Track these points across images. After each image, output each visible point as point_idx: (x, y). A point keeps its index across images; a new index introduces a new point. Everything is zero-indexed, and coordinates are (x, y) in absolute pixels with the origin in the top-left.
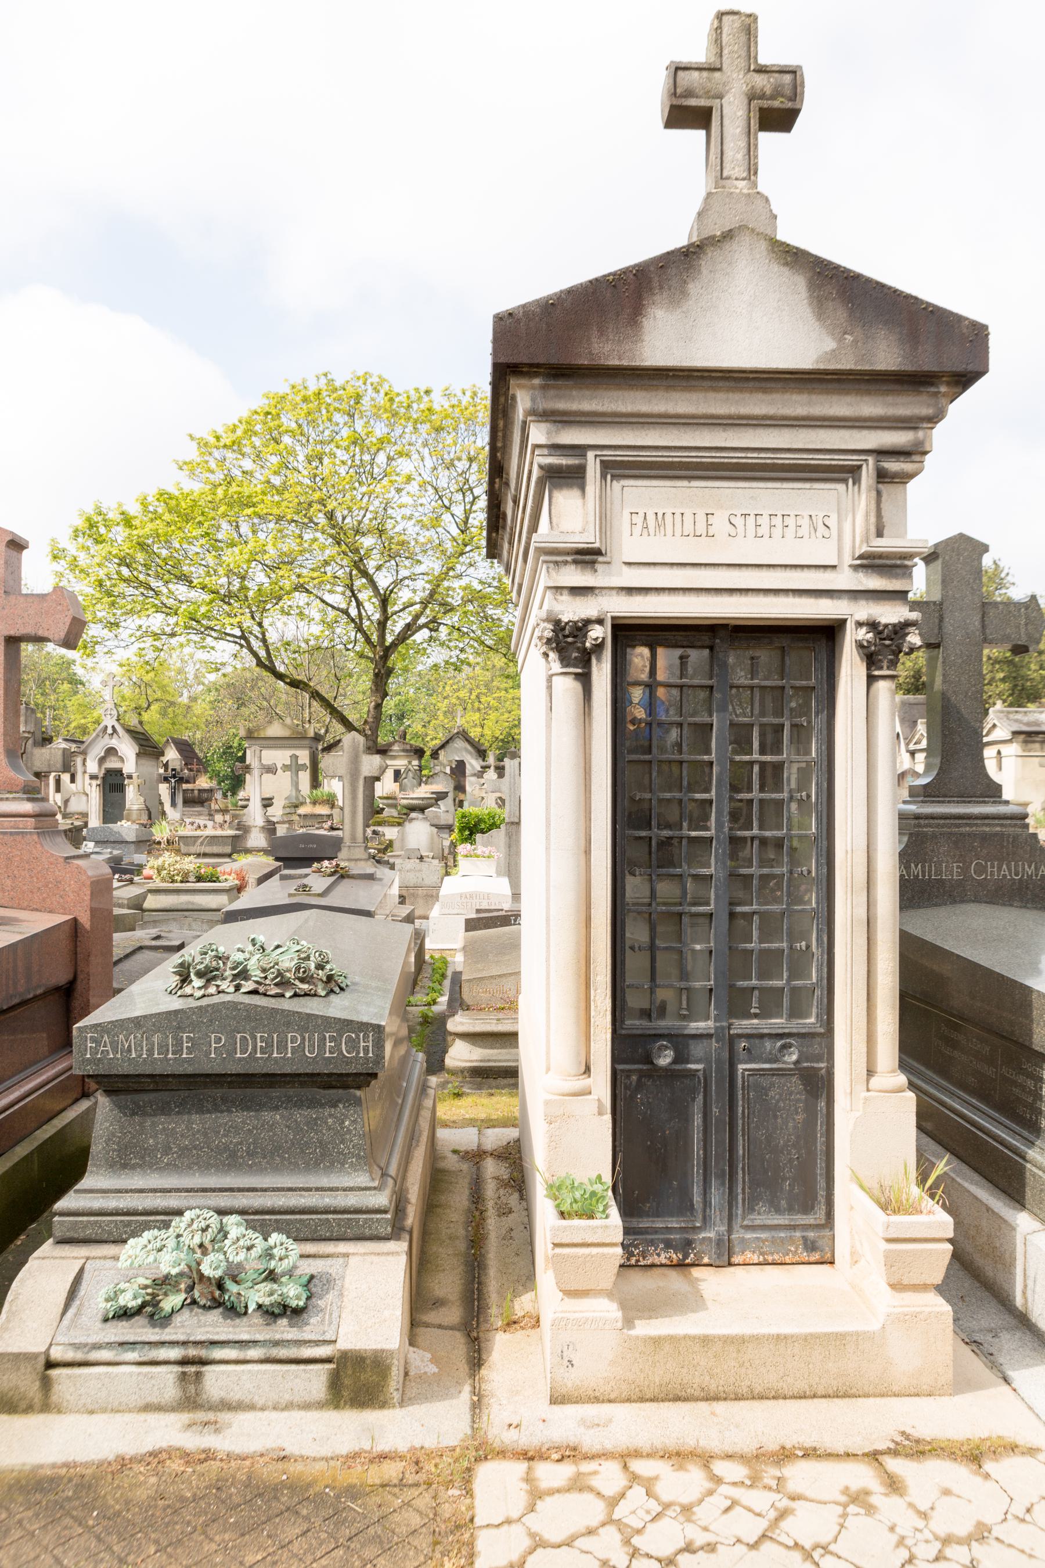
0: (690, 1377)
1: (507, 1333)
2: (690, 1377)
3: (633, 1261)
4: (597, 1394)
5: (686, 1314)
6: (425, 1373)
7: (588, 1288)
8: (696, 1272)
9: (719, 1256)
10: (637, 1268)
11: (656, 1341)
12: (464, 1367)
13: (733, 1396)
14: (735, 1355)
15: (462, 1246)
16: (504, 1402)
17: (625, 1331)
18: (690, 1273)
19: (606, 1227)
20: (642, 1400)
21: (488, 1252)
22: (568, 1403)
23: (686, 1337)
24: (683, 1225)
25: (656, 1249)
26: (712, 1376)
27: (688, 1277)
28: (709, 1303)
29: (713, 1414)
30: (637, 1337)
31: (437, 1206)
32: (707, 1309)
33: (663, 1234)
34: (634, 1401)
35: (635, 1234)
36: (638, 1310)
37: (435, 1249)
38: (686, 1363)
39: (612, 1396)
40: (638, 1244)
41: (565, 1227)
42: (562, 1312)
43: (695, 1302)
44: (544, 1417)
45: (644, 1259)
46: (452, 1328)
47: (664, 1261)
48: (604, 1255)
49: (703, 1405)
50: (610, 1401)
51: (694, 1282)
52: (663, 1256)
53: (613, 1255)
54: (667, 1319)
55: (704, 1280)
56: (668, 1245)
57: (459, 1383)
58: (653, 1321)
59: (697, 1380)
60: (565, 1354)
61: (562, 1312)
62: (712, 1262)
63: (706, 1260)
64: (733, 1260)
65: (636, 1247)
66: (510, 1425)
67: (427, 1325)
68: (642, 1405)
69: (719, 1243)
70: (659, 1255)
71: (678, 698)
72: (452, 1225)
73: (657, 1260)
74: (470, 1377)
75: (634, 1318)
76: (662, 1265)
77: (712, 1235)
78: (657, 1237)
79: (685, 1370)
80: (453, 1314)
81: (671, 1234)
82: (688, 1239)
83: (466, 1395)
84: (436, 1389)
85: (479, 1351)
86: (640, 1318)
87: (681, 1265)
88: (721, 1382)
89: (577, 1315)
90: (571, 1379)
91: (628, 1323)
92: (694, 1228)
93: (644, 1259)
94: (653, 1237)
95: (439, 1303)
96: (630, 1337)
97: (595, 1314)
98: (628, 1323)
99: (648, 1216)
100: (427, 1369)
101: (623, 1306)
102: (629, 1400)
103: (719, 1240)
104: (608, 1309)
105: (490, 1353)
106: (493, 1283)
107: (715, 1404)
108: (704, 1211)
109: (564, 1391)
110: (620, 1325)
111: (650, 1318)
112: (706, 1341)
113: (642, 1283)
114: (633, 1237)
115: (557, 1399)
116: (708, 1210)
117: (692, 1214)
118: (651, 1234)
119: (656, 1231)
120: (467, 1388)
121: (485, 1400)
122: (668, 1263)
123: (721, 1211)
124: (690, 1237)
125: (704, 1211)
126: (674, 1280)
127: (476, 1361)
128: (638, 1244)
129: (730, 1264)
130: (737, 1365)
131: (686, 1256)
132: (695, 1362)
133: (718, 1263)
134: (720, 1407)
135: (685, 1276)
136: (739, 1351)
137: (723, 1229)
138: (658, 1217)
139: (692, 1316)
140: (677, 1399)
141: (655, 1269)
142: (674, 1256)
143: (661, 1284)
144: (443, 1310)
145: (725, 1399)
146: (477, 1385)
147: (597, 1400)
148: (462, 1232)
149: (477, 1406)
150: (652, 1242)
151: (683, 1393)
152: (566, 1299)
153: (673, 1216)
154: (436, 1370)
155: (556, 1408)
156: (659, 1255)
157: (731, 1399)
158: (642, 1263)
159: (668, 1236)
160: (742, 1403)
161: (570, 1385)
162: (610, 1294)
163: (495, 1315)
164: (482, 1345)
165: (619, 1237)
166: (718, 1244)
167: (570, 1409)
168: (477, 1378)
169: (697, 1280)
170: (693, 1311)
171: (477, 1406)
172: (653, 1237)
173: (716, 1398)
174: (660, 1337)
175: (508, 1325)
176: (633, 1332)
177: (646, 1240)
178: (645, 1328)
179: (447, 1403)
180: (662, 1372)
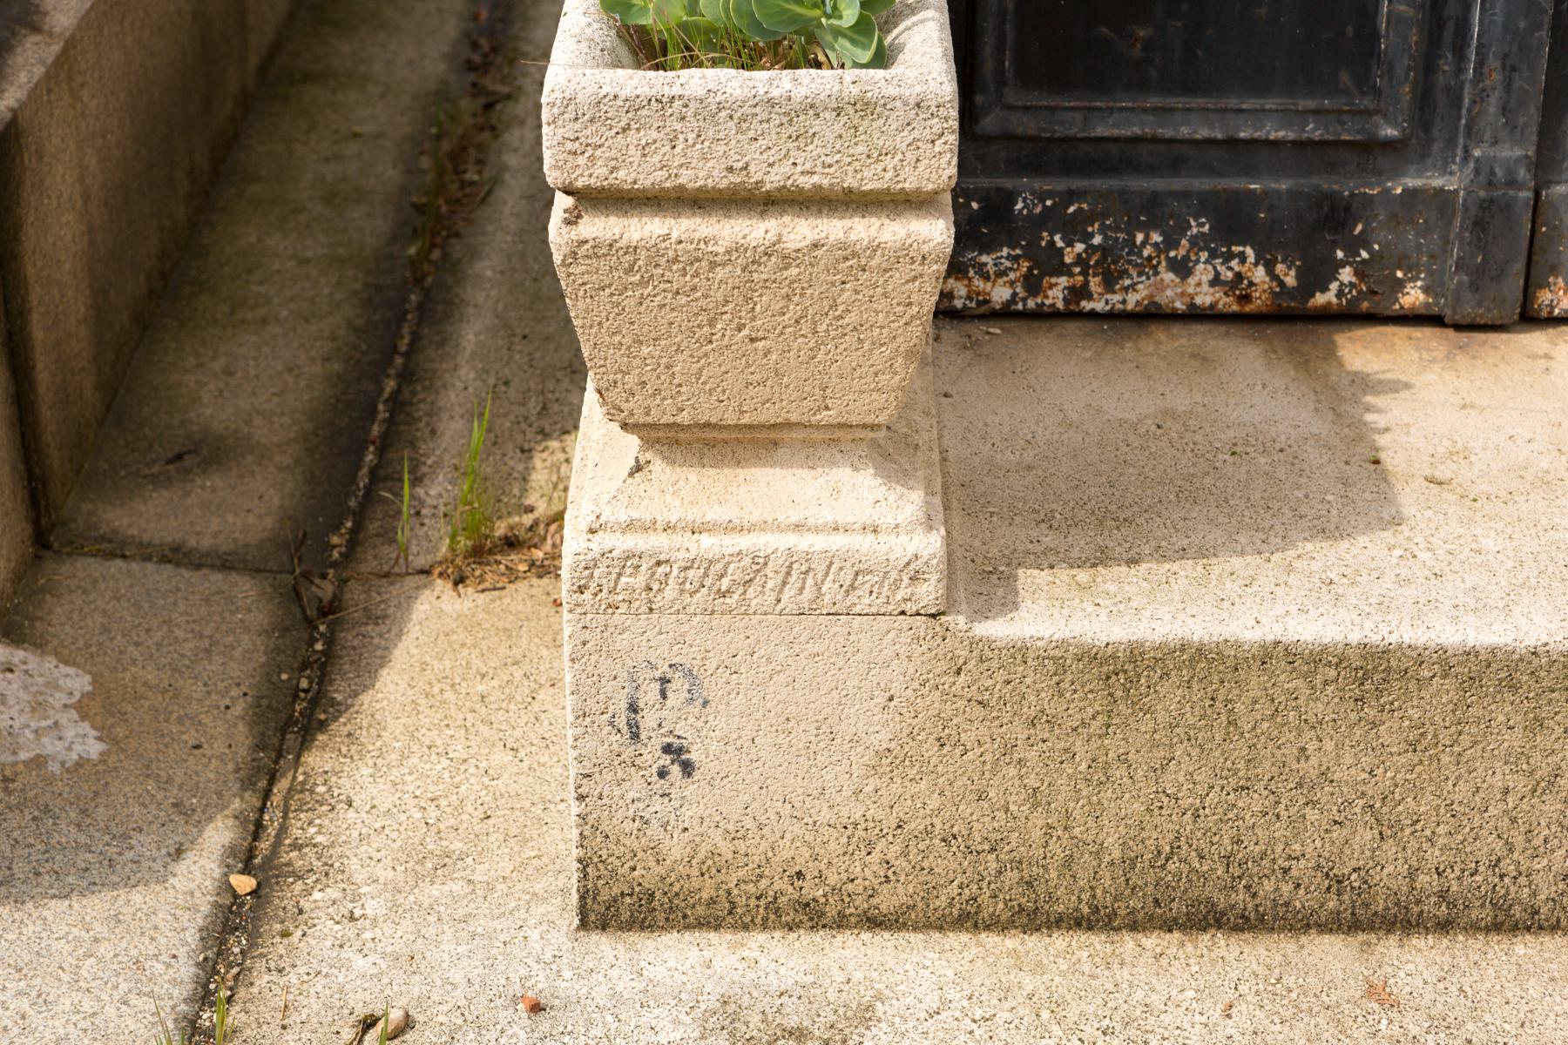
0: (1280, 831)
1: (469, 591)
2: (1280, 831)
3: (1056, 293)
4: (811, 891)
5: (1287, 542)
6: (39, 761)
7: (767, 415)
8: (1361, 352)
9: (1480, 277)
10: (1071, 327)
11: (1122, 673)
12: (229, 737)
13: (1485, 914)
14: (1514, 740)
15: (370, 227)
16: (372, 907)
17: (959, 621)
18: (1331, 352)
19: (865, 107)
20: (1033, 918)
21: (475, 254)
22: (668, 925)
23: (1271, 656)
24: (1313, 131)
25: (1171, 243)
26: (1386, 830)
27: (1316, 369)
28: (1409, 497)
29: (1379, 993)
30: (1020, 652)
31: (308, 78)
32: (1396, 521)
33: (1209, 170)
34: (995, 925)
35: (1069, 167)
36: (1047, 521)
37: (1128, 345)
38: (1267, 768)
39: (887, 902)
40: (1084, 219)
41: (634, 106)
42: (630, 527)
43: (1350, 487)
44: (541, 984)
45: (1109, 286)
46: (226, 562)
47: (1206, 297)
48: (847, 252)
49: (1332, 956)
50: (874, 922)
51: (1345, 399)
52: (1203, 273)
53: (904, 253)
54: (1186, 569)
55: (1396, 387)
56: (1233, 224)
57: (190, 815)
58: (1113, 578)
59: (1312, 845)
60: (648, 720)
61: (630, 527)
62: (1441, 306)
63: (1413, 296)
64: (1545, 297)
65: (1075, 229)
66: (368, 1023)
67: (116, 548)
68: (1033, 941)
69: (1486, 216)
70: (1182, 269)
71: (1388, 313)
72: (352, 148)
73: (1170, 290)
74: (247, 784)
75: (1016, 560)
76: (1196, 316)
77: (1452, 181)
78: (1177, 184)
79: (1256, 801)
80: (247, 505)
81: (1251, 171)
82: (1332, 197)
83: (202, 870)
84: (67, 833)
85: (323, 666)
86: (1046, 559)
87: (1293, 320)
88: (1434, 856)
89: (708, 544)
90: (685, 827)
91: (980, 577)
92: (1370, 148)
93: (1109, 286)
94: (1159, 184)
95: (198, 454)
96: (983, 650)
97: (804, 542)
98: (980, 577)
99: (1142, 85)
100: (49, 745)
101: (960, 498)
102: (968, 920)
103: (1487, 205)
104: (871, 517)
105: (367, 674)
106: (466, 373)
107: (1389, 946)
108: (1428, 66)
109: (648, 874)
110: (928, 593)
111: (1101, 559)
112: (1371, 674)
113: (1078, 394)
114: (1061, 184)
115: (616, 905)
116: (1446, 65)
117: (1364, 83)
118: (1152, 171)
119: (1176, 155)
120: (219, 834)
121: (288, 894)
122: (1228, 303)
123: (1510, 69)
124: (1345, 187)
125: (1428, 66)
126: (1251, 389)
127: (299, 704)
128: (1084, 219)
129: (1530, 318)
130: (1520, 784)
131: (1317, 276)
132: (1310, 767)
133: (1468, 311)
134: (1414, 964)
135: (1304, 365)
136: (1538, 724)
137: (1513, 152)
138: (1191, 89)
139: (1322, 557)
140: (1206, 919)
141: (1159, 332)
142: (1260, 274)
143: (1181, 400)
144: (212, 486)
145: (1444, 926)
146: (272, 819)
147: (811, 916)
148: (387, 172)
149: (238, 928)
150: (1153, 211)
151: (1241, 897)
152: (658, 465)
153: (1265, 90)
154: (94, 749)
155: (604, 945)
156: (1182, 269)
157: (1474, 928)
158: (1098, 306)
159: (1236, 183)
160: (1524, 948)
161: (675, 848)
162: (887, 447)
163: (436, 500)
164: (347, 637)
165: (938, 166)
166: (1479, 225)
167: (674, 957)
168: (282, 785)
169: (1364, 383)
170: (1324, 531)
171: (238, 928)
172: (1159, 184)
173: (1402, 920)
174: (1136, 653)
175: (479, 553)
176: (998, 629)
177: (1124, 196)
178: (1058, 611)
179: (95, 906)
180: (1120, 814)
